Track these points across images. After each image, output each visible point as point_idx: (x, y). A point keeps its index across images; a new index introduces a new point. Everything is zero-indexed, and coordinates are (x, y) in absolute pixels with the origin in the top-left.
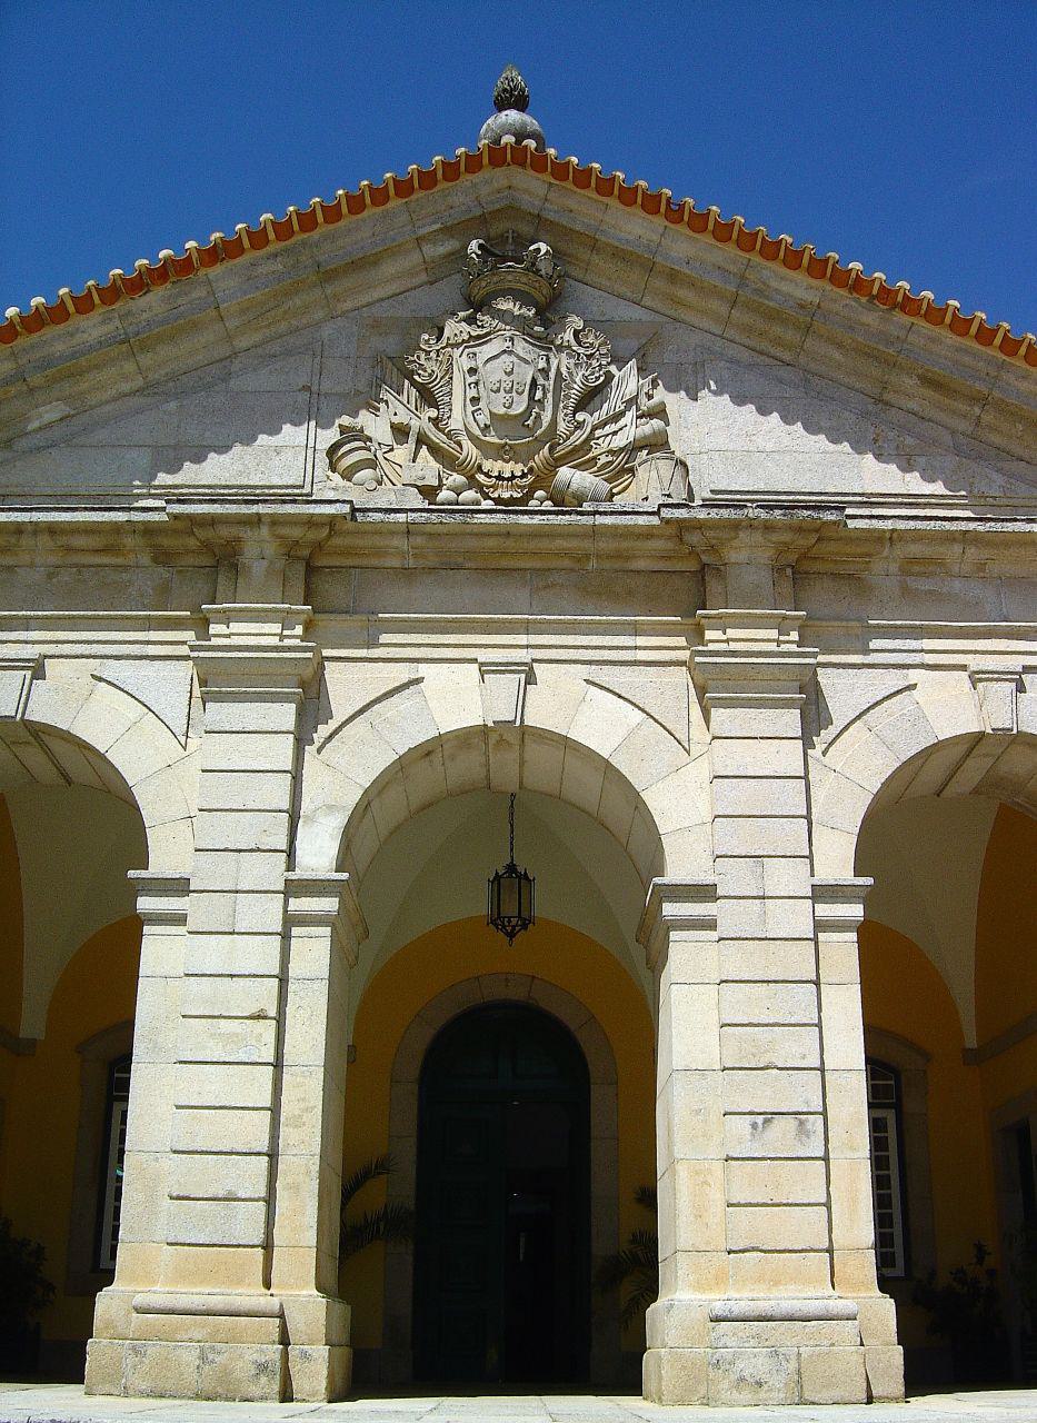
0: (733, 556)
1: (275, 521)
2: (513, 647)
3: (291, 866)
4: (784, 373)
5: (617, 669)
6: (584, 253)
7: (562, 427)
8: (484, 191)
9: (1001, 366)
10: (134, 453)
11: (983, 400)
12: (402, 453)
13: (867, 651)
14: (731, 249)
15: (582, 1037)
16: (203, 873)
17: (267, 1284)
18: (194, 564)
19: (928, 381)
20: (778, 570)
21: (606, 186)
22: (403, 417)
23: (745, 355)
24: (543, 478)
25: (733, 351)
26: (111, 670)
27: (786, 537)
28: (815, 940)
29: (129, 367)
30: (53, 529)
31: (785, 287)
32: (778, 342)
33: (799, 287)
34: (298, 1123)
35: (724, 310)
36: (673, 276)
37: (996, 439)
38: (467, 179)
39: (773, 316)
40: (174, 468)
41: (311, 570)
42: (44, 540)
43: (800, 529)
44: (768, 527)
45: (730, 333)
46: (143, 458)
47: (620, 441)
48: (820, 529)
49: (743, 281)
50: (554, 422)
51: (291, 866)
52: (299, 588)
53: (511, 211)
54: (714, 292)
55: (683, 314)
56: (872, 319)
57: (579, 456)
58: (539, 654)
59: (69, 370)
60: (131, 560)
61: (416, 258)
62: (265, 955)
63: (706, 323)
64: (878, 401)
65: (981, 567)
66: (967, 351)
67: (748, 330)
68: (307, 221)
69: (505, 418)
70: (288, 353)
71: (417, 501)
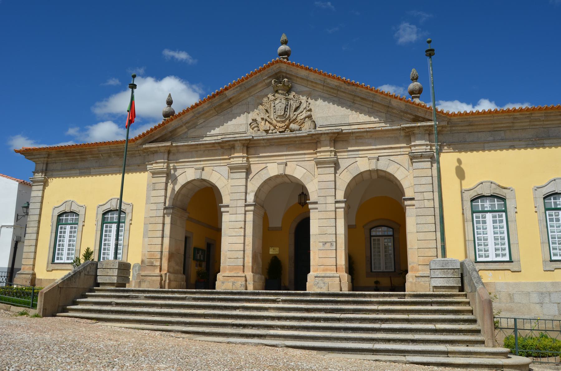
0: (322, 139)
1: (240, 140)
2: (283, 159)
3: (246, 202)
6: (295, 78)
7: (291, 116)
8: (275, 68)
9: (375, 95)
11: (373, 102)
14: (321, 76)
16: (231, 204)
17: (244, 272)
20: (330, 141)
21: (297, 66)
22: (262, 117)
24: (288, 127)
26: (216, 168)
27: (331, 135)
28: (336, 211)
31: (332, 82)
32: (333, 93)
33: (335, 83)
34: (248, 245)
35: (322, 87)
36: (312, 82)
37: (376, 109)
38: (271, 67)
47: (302, 117)
49: (324, 82)
50: (290, 115)
51: (246, 202)
52: (245, 151)
53: (280, 72)
57: (294, 121)
58: (287, 160)
60: (217, 148)
61: (264, 83)
62: (241, 217)
63: (320, 90)
64: (353, 103)
66: (368, 92)
67: (327, 91)
68: (243, 80)
69: (280, 116)
71: (264, 134)
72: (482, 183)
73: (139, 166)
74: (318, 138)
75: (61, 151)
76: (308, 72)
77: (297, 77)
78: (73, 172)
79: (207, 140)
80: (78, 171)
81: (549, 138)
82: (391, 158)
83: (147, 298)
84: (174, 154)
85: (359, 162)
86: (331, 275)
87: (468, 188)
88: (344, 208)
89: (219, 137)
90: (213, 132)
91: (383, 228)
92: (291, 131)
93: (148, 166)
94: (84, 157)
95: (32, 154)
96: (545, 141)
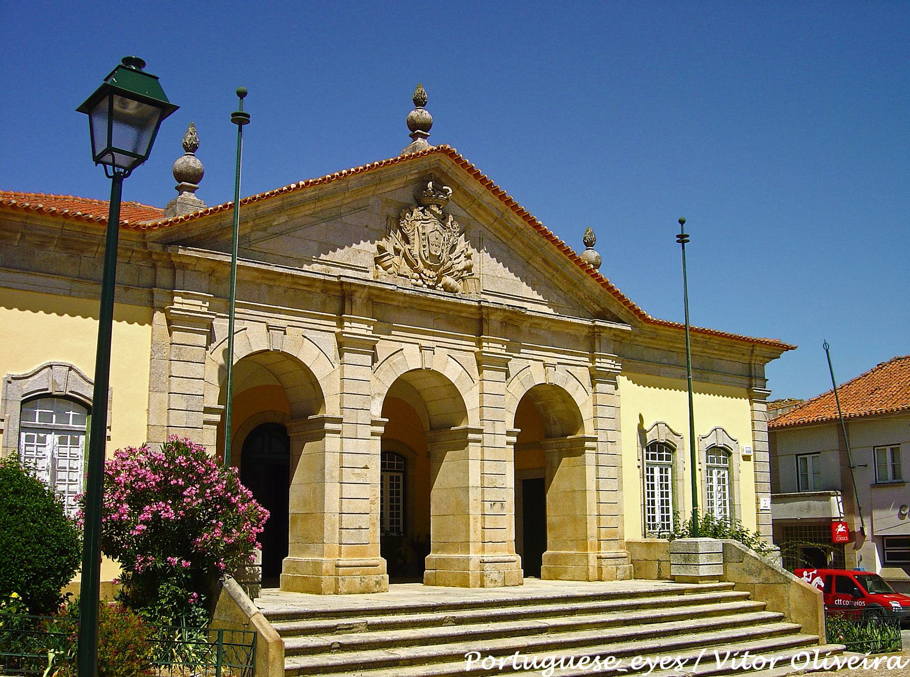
1: (370, 287)
4: (502, 246)
5: (95, 134)
9: (568, 262)
10: (311, 244)
11: (557, 270)
12: (397, 259)
13: (520, 353)
14: (503, 204)
18: (340, 299)
19: (545, 261)
23: (493, 238)
30: (292, 275)
33: (519, 222)
35: (492, 221)
36: (480, 205)
39: (506, 228)
40: (326, 254)
45: (490, 229)
46: (315, 246)
54: (492, 215)
55: (479, 219)
56: (536, 238)
64: (527, 262)
72: (51, 366)
79: (313, 270)
82: (569, 368)
85: (533, 369)
88: (515, 444)
89: (337, 271)
90: (331, 256)
93: (176, 299)
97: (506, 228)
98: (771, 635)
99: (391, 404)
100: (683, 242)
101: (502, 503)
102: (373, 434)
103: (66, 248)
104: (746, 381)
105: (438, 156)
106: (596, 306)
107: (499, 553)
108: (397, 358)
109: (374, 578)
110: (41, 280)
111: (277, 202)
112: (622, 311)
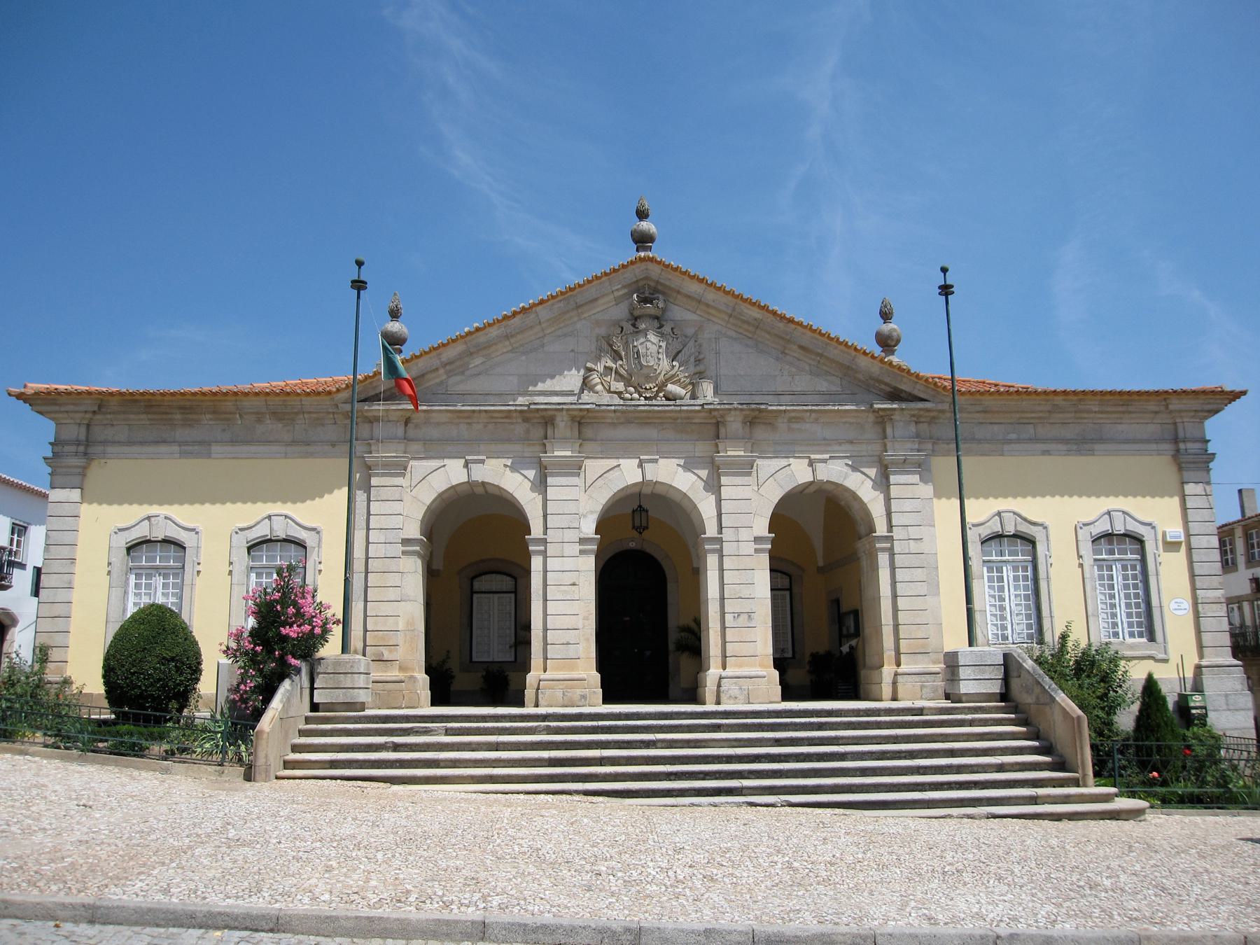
1: (568, 410)
11: (821, 355)
15: (664, 564)
19: (802, 348)
25: (730, 333)
29: (507, 343)
30: (486, 411)
33: (755, 313)
36: (708, 305)
41: (580, 423)
42: (483, 415)
43: (753, 410)
44: (742, 410)
48: (760, 410)
49: (734, 309)
56: (781, 325)
59: (488, 345)
61: (611, 297)
64: (783, 352)
65: (817, 419)
70: (565, 335)
73: (333, 446)
74: (722, 416)
75: (136, 401)
76: (703, 286)
77: (679, 292)
78: (163, 449)
80: (176, 448)
81: (1101, 440)
83: (448, 732)
84: (417, 426)
86: (753, 674)
87: (975, 521)
90: (540, 387)
91: (499, 577)
92: (668, 399)
94: (195, 417)
95: (54, 402)
96: (1097, 447)
97: (745, 322)
98: (1001, 768)
99: (777, 521)
100: (947, 295)
101: (750, 615)
102: (582, 552)
103: (280, 420)
104: (1168, 447)
105: (643, 266)
106: (883, 387)
107: (746, 669)
108: (615, 473)
109: (579, 692)
110: (261, 449)
111: (460, 348)
112: (918, 386)
